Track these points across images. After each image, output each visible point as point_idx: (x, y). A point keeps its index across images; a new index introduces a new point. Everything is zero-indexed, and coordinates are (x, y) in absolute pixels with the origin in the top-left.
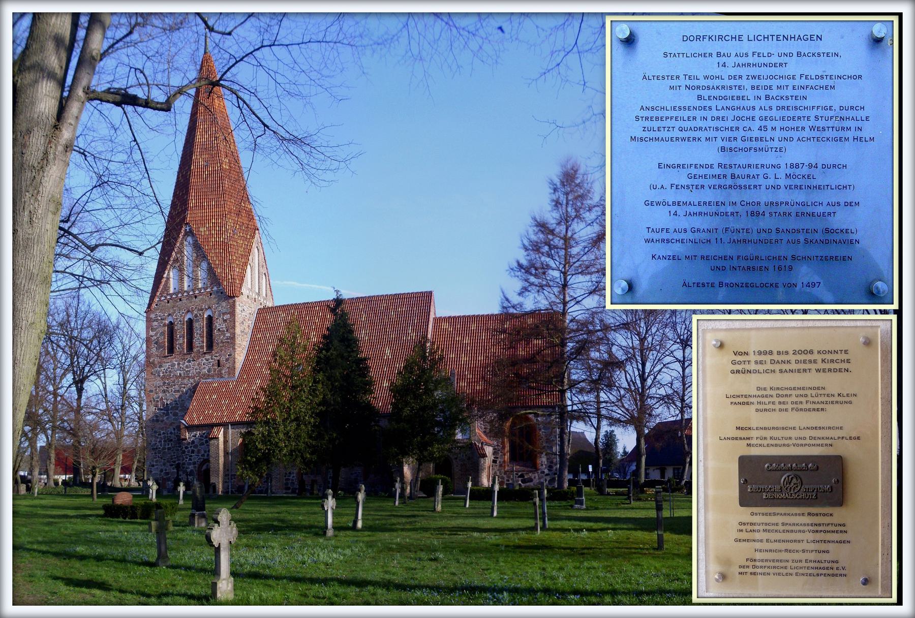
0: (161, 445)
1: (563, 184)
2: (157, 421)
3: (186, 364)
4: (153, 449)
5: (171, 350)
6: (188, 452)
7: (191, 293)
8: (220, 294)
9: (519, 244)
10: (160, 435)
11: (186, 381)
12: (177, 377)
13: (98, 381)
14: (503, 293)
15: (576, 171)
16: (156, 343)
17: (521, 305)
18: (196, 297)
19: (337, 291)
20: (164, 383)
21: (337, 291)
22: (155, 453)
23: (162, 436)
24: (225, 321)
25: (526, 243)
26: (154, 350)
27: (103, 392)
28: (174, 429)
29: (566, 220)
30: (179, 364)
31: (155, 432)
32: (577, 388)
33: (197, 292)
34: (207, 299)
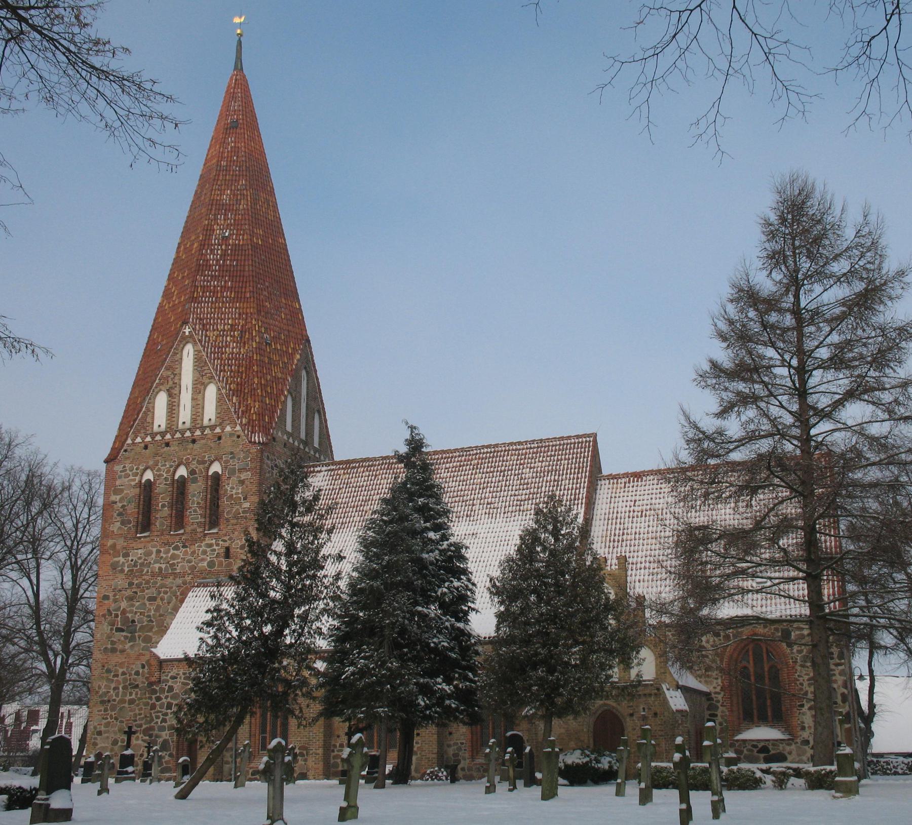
0: (117, 695)
1: (783, 220)
2: (114, 650)
3: (172, 551)
4: (103, 702)
5: (145, 524)
6: (162, 706)
7: (188, 434)
8: (235, 438)
9: (709, 330)
10: (117, 676)
11: (169, 581)
12: (153, 575)
13: (25, 582)
14: (687, 418)
15: (808, 197)
16: (120, 514)
17: (720, 433)
18: (194, 441)
19: (412, 428)
20: (131, 584)
21: (412, 428)
22: (106, 710)
23: (120, 678)
24: (242, 482)
25: (723, 326)
26: (116, 527)
27: (32, 600)
28: (143, 667)
29: (795, 283)
30: (159, 552)
31: (109, 671)
32: (863, 589)
33: (198, 433)
34: (212, 445)
